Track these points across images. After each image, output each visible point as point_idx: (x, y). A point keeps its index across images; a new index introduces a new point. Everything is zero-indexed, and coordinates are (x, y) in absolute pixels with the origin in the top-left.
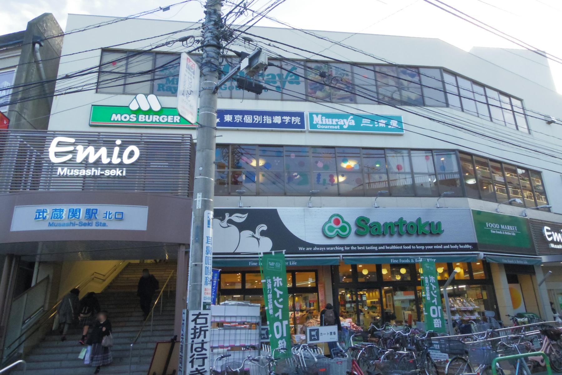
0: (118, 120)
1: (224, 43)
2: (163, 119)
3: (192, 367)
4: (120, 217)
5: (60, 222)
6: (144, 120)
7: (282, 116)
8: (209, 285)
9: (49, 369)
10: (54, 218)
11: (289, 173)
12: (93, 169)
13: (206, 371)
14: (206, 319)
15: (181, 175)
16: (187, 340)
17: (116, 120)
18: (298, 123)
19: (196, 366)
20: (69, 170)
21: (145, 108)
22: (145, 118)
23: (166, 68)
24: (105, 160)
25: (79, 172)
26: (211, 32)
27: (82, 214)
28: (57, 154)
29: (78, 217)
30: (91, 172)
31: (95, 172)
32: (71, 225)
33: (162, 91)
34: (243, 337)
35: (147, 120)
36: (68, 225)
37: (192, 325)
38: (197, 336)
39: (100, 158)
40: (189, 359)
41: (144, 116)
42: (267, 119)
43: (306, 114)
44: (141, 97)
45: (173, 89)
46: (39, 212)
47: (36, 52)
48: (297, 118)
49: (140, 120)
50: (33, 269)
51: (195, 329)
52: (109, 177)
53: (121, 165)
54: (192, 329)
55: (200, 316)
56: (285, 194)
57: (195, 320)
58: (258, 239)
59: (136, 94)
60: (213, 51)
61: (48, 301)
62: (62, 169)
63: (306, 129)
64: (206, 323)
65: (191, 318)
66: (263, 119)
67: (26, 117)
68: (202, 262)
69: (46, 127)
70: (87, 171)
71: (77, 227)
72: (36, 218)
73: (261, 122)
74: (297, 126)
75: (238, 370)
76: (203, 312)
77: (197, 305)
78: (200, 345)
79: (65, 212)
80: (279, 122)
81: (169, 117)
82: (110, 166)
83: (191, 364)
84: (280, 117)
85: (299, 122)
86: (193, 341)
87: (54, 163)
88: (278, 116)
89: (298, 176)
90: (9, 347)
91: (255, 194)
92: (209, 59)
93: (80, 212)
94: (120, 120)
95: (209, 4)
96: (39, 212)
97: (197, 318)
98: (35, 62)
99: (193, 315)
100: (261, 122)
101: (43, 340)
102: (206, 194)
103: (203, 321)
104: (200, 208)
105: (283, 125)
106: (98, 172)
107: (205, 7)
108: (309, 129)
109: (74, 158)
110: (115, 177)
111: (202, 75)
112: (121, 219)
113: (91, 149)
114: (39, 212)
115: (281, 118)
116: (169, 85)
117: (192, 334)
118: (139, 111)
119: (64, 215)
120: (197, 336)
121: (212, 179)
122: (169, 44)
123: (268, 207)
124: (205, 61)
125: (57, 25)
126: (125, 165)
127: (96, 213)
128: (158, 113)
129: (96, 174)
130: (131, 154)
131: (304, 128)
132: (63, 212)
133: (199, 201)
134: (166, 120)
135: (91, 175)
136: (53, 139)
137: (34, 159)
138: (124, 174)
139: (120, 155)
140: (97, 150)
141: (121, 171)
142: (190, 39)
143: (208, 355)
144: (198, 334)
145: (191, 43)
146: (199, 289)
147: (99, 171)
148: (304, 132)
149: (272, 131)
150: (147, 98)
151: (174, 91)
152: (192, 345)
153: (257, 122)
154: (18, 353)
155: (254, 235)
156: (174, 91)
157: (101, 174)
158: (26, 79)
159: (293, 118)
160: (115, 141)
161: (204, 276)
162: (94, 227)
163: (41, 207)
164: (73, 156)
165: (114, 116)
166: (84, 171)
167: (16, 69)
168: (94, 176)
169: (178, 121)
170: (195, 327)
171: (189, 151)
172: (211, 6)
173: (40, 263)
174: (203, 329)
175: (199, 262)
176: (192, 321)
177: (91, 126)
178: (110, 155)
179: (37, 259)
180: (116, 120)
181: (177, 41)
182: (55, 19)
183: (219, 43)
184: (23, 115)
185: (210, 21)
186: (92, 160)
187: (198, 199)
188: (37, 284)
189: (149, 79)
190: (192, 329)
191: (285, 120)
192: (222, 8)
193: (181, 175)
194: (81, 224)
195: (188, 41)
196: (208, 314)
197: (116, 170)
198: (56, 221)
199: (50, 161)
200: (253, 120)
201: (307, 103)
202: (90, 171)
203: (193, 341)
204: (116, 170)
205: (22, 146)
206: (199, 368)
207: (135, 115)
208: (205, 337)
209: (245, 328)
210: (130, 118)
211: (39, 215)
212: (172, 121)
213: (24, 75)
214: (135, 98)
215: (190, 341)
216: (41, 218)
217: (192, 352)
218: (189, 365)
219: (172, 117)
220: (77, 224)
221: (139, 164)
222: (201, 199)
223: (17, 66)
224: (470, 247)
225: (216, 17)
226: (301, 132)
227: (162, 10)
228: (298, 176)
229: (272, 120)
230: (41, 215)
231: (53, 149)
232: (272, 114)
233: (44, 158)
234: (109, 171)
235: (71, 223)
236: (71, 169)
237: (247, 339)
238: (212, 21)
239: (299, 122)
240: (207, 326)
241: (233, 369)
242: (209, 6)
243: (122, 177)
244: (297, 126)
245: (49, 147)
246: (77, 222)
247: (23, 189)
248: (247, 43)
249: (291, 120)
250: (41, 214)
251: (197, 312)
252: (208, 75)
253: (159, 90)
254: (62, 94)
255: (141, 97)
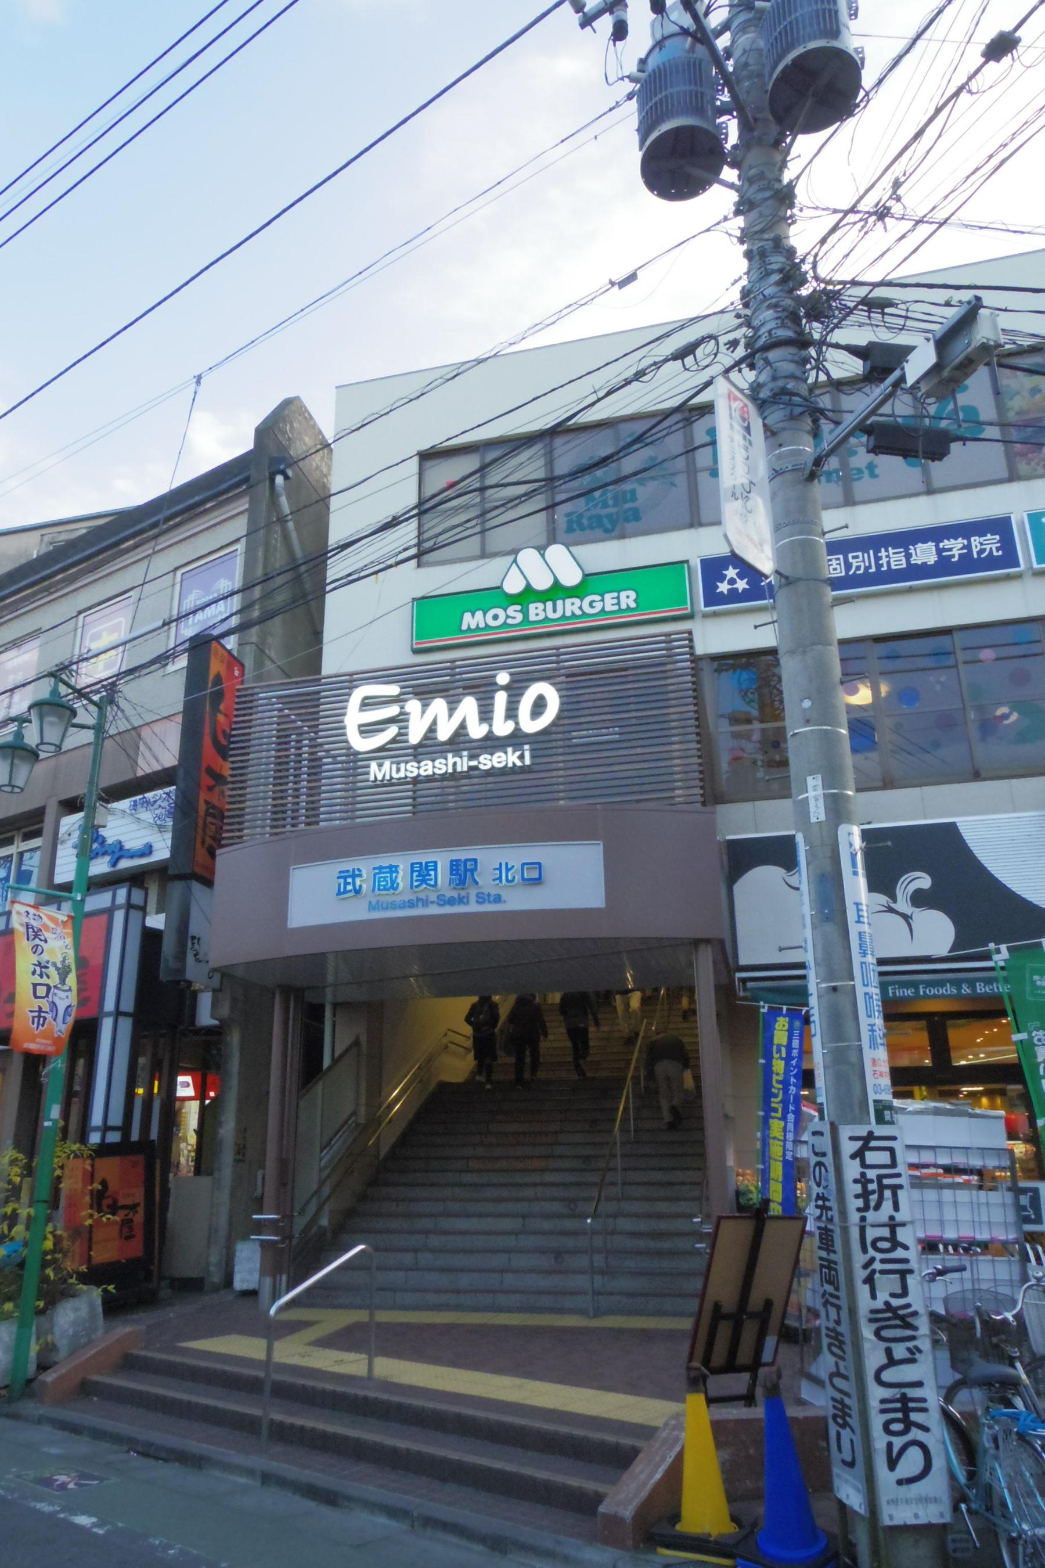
0: (478, 628)
1: (816, 330)
2: (590, 605)
3: (874, 1296)
4: (535, 875)
5: (394, 898)
6: (542, 616)
7: (938, 541)
8: (881, 1047)
9: (390, 1269)
10: (379, 889)
11: (980, 709)
12: (450, 755)
13: (915, 1314)
14: (892, 1151)
15: (676, 747)
16: (843, 1213)
17: (473, 626)
18: (995, 554)
19: (883, 1296)
20: (394, 766)
21: (542, 582)
22: (545, 610)
23: (648, 441)
24: (477, 731)
25: (419, 768)
26: (775, 306)
27: (442, 875)
28: (366, 730)
29: (432, 883)
30: (446, 765)
31: (455, 764)
32: (420, 904)
33: (578, 532)
34: (965, 1215)
35: (551, 615)
36: (411, 904)
37: (852, 1169)
38: (872, 1204)
39: (463, 726)
40: (860, 1274)
41: (541, 606)
42: (894, 559)
43: (1019, 519)
44: (528, 557)
45: (605, 521)
46: (345, 878)
47: (279, 496)
48: (989, 536)
49: (532, 618)
50: (322, 1022)
51: (863, 1180)
52: (492, 772)
53: (517, 739)
54: (856, 1181)
55: (874, 1144)
56: (977, 776)
57: (860, 1154)
58: (907, 918)
59: (515, 552)
60: (790, 357)
61: (363, 1100)
62: (380, 765)
63: (1023, 566)
64: (894, 1164)
65: (848, 1147)
66: (878, 559)
67: (273, 654)
68: (853, 979)
69: (318, 670)
70: (437, 763)
71: (434, 910)
72: (339, 893)
73: (873, 570)
74: (989, 562)
75: (1009, 1316)
76: (880, 1130)
77: (857, 1111)
78: (885, 1232)
79: (401, 873)
80: (932, 559)
81: (607, 596)
82: (492, 743)
83: (867, 1287)
84: (931, 545)
85: (998, 549)
86: (863, 1219)
87: (360, 753)
88: (925, 542)
89: (1014, 716)
90: (302, 1211)
91: (880, 784)
92: (780, 383)
93: (435, 870)
94: (482, 625)
95: (757, 228)
96: (343, 875)
97: (865, 1148)
98: (278, 520)
99: (852, 1138)
100: (873, 570)
101: (363, 1198)
102: (832, 777)
103: (884, 1158)
104: (822, 817)
105: (944, 566)
106: (463, 764)
107: (741, 241)
108: (1035, 566)
109: (403, 734)
110: (504, 771)
111: (770, 432)
112: (538, 881)
113: (439, 705)
114: (343, 875)
115: (937, 546)
116: (594, 512)
117: (857, 1196)
118: (529, 594)
119: (402, 879)
120: (872, 1204)
121: (844, 731)
122: (645, 374)
123: (926, 818)
124: (768, 393)
125: (312, 423)
126: (527, 735)
127: (476, 869)
128: (575, 592)
129: (459, 769)
130: (539, 706)
131: (1018, 565)
132: (397, 872)
133: (816, 799)
134: (598, 606)
135: (446, 773)
136: (349, 695)
137: (306, 749)
138: (528, 761)
139: (512, 713)
140: (452, 707)
141: (518, 753)
142: (703, 346)
143: (914, 1265)
144: (874, 1198)
145: (709, 355)
146: (854, 1059)
147: (465, 759)
148: (1019, 576)
149: (911, 590)
150: (543, 556)
151: (609, 526)
152: (862, 1231)
153: (861, 571)
154: (320, 1227)
155: (893, 905)
156: (609, 526)
157: (471, 768)
158: (265, 567)
159: (975, 541)
160: (494, 676)
161: (864, 1021)
162: (473, 907)
163: (348, 865)
164: (400, 728)
165: (467, 616)
166: (430, 763)
167: (240, 547)
168: (454, 776)
169: (633, 605)
170: (863, 1175)
171: (689, 678)
172: (762, 231)
173: (335, 1006)
174: (886, 1182)
175: (842, 979)
176: (853, 1157)
177: (416, 652)
178: (486, 715)
179: (329, 997)
180: (473, 626)
181: (666, 360)
182: (306, 410)
183: (801, 333)
184: (267, 652)
185: (768, 274)
186: (444, 734)
187: (811, 794)
188: (335, 1061)
189: (543, 505)
190: (856, 1181)
191: (950, 550)
192: (793, 230)
193: (676, 747)
194: (443, 901)
195: (699, 352)
196: (894, 1138)
197: (506, 753)
198: (387, 897)
199: (351, 748)
200: (848, 566)
201: (1016, 487)
202: (444, 761)
203: (863, 1219)
204: (506, 753)
205: (283, 720)
206: (895, 1302)
207: (519, 607)
208: (896, 1208)
209: (966, 1185)
210: (508, 617)
211: (346, 884)
212: (616, 608)
213: (260, 554)
214: (515, 561)
215: (854, 1217)
216: (350, 891)
217: (865, 1250)
218: (864, 1291)
219: (615, 595)
220: (433, 902)
221: (560, 729)
222: (820, 792)
223: (244, 540)
224: (81, 1062)
225: (782, 259)
226: (1008, 578)
227: (616, 287)
228: (1014, 716)
229: (908, 556)
230: (349, 884)
231: (354, 717)
232: (905, 539)
233: (321, 745)
234: (489, 757)
235: (418, 899)
236: (398, 763)
237: (976, 1219)
238: (773, 272)
239: (998, 549)
240: (899, 1175)
241: (999, 1314)
242: (756, 233)
243: (524, 769)
244: (989, 562)
245: (344, 715)
246: (433, 897)
247: (293, 826)
248: (876, 316)
249: (968, 547)
250: (350, 880)
251: (862, 1131)
252: (784, 429)
253: (570, 530)
254: (391, 566)
255: (528, 557)
